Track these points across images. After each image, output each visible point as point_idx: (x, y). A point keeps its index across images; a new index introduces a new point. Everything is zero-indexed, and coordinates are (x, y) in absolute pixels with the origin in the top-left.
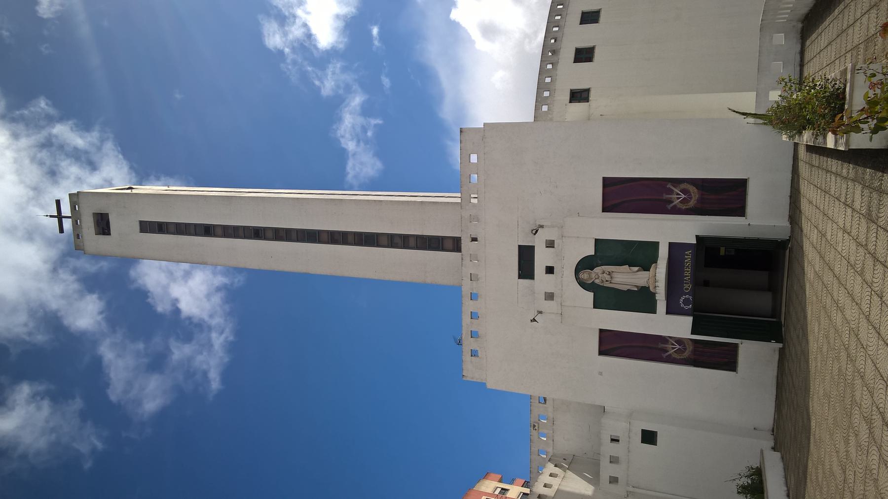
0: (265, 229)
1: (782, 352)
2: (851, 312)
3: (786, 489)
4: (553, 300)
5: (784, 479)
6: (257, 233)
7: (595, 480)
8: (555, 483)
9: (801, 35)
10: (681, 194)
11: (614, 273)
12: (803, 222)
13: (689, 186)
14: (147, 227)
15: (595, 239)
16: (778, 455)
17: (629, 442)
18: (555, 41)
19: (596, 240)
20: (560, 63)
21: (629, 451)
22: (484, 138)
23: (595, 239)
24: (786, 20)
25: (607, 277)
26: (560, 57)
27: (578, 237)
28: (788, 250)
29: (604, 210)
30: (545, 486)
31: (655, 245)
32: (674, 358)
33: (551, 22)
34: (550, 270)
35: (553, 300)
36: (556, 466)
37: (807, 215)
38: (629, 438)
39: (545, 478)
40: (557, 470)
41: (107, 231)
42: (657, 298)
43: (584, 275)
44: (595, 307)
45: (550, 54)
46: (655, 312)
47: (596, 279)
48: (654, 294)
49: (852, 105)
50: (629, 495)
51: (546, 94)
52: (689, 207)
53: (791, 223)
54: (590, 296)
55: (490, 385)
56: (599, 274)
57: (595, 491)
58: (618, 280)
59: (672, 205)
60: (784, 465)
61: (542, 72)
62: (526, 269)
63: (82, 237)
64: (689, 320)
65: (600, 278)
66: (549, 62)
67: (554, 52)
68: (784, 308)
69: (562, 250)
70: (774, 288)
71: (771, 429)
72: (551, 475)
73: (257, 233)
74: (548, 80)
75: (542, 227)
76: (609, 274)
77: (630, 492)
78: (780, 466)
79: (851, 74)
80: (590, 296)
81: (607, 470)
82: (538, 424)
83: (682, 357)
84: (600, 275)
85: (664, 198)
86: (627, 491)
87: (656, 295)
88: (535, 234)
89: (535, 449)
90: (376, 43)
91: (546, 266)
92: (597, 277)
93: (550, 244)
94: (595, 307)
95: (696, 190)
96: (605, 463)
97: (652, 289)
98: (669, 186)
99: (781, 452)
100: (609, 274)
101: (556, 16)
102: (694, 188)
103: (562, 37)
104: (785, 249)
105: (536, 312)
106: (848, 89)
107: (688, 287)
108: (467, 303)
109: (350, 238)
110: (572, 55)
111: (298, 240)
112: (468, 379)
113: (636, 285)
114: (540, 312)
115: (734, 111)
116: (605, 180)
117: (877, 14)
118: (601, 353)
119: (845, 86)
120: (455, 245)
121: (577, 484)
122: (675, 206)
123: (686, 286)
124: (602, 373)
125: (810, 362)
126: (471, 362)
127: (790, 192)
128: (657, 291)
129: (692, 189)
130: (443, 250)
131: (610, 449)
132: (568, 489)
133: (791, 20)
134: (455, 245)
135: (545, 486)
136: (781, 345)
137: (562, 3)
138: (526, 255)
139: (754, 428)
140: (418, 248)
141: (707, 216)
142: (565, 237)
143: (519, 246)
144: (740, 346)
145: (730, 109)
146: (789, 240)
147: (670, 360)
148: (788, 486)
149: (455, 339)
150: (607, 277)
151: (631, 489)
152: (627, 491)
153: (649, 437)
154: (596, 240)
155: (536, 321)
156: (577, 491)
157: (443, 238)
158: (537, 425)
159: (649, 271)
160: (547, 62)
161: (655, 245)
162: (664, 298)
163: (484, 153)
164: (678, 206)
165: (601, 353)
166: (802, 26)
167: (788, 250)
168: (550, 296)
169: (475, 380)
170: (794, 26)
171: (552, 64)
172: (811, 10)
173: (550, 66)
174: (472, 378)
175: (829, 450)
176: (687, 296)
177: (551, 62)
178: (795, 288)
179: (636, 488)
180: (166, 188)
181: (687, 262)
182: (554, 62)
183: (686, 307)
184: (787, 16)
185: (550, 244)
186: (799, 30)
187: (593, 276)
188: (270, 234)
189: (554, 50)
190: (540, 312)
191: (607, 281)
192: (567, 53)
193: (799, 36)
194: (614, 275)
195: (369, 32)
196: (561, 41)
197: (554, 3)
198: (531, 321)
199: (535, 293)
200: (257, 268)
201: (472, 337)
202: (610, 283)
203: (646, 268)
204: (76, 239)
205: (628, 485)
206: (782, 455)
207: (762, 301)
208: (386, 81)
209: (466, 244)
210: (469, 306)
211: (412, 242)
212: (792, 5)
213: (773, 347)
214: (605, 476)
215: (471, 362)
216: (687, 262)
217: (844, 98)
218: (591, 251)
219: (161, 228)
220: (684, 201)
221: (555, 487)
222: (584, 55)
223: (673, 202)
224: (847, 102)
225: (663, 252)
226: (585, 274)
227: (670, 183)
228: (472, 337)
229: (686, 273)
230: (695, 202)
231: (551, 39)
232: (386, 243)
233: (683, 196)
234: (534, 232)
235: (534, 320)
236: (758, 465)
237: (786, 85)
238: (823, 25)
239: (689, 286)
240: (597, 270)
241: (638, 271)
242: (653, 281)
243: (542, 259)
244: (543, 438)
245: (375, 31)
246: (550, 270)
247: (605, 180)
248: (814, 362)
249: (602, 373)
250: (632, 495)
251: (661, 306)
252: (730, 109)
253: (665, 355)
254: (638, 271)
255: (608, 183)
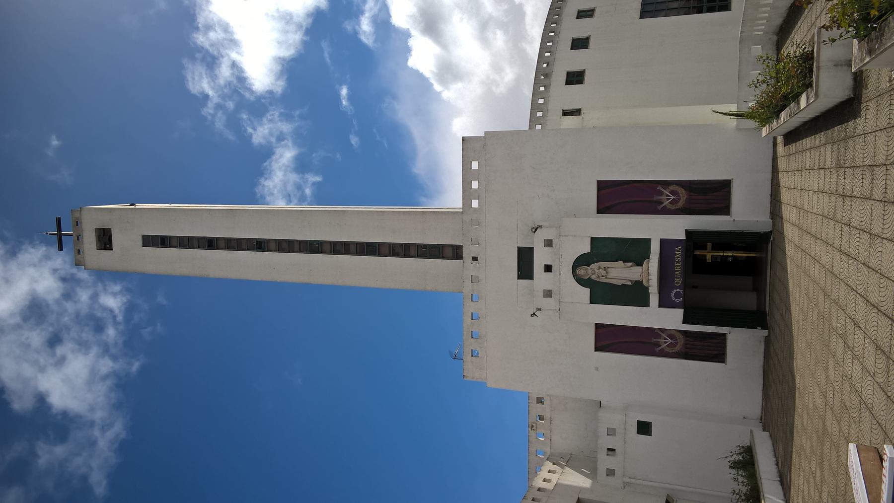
0: (268, 241)
1: (768, 341)
2: (825, 255)
3: (775, 459)
4: (551, 297)
5: (773, 452)
6: (260, 245)
7: (592, 474)
8: (554, 478)
9: (776, 47)
10: (670, 195)
11: (609, 269)
12: (783, 210)
13: (677, 187)
14: (149, 241)
15: (591, 238)
16: (767, 434)
17: (625, 434)
18: (547, 66)
19: (592, 238)
20: (551, 87)
21: (625, 443)
22: (485, 145)
23: (591, 238)
24: (762, 33)
25: (603, 273)
26: (552, 79)
27: (575, 236)
28: (770, 243)
29: (599, 211)
30: (544, 480)
31: (647, 242)
32: (667, 352)
33: (543, 48)
34: (548, 268)
35: (551, 297)
36: (554, 464)
37: (790, 238)
38: (625, 429)
39: (544, 474)
40: (555, 467)
41: (108, 246)
42: (650, 291)
43: (581, 271)
44: (591, 303)
45: (542, 77)
46: (648, 306)
47: (593, 274)
48: (647, 288)
49: (819, 61)
50: (626, 487)
51: (540, 114)
52: (678, 207)
53: (772, 219)
54: (586, 292)
55: (491, 384)
56: (595, 271)
57: (593, 484)
58: (612, 275)
59: (662, 206)
60: (772, 441)
61: (536, 94)
62: (525, 267)
63: (83, 252)
64: (681, 311)
65: (596, 274)
66: (541, 85)
67: (547, 76)
68: (768, 298)
69: (559, 248)
70: (758, 289)
71: (760, 417)
72: (549, 471)
73: (260, 245)
74: (541, 101)
75: (540, 227)
76: (605, 269)
77: (627, 482)
78: (769, 443)
79: (818, 36)
80: (586, 292)
81: (605, 462)
82: (536, 424)
83: (674, 351)
84: (597, 271)
85: (655, 199)
86: (624, 482)
87: (649, 288)
88: (535, 232)
89: (533, 450)
90: (344, 102)
91: (545, 265)
92: (593, 272)
93: (549, 243)
94: (591, 303)
95: (684, 191)
96: (602, 455)
97: (645, 283)
98: (659, 188)
99: (769, 432)
100: (605, 269)
101: (547, 42)
102: (683, 190)
103: (554, 61)
104: (767, 242)
105: (535, 309)
106: (815, 50)
107: (678, 281)
108: (468, 305)
109: (353, 248)
110: (563, 78)
111: (300, 251)
112: (468, 379)
113: (630, 279)
114: (539, 309)
115: (718, 112)
116: (599, 183)
117: (866, 118)
118: (597, 349)
119: (813, 47)
120: (456, 252)
121: (576, 479)
122: (665, 206)
123: (677, 280)
124: (597, 368)
125: (793, 328)
126: (472, 362)
127: (770, 191)
128: (650, 284)
129: (681, 191)
130: (443, 257)
131: (607, 442)
132: (566, 483)
133: (767, 33)
134: (456, 252)
135: (544, 480)
136: (765, 333)
137: (553, 30)
138: (525, 258)
139: (744, 417)
140: (418, 256)
141: (695, 216)
142: (563, 236)
143: (519, 248)
144: (729, 337)
145: (713, 111)
146: (771, 232)
147: (663, 354)
148: (777, 457)
149: (450, 353)
150: (603, 273)
151: (627, 480)
152: (624, 482)
153: (644, 428)
154: (592, 238)
155: (536, 315)
156: (575, 484)
157: (443, 246)
158: (534, 425)
159: (642, 266)
160: (540, 85)
161: (647, 242)
162: (657, 292)
163: (485, 160)
164: (668, 207)
165: (597, 349)
166: (777, 38)
167: (770, 243)
168: (548, 294)
169: (475, 380)
170: (770, 39)
171: (544, 86)
172: (784, 21)
173: (542, 89)
174: (473, 378)
175: (811, 391)
176: (678, 290)
177: (544, 84)
178: (778, 274)
179: (632, 478)
180: (169, 205)
181: (677, 258)
182: (546, 84)
183: (677, 301)
184: (764, 27)
185: (549, 243)
186: (775, 43)
187: (590, 271)
188: (273, 246)
189: (547, 74)
190: (539, 309)
191: (602, 276)
192: (559, 77)
193: (775, 48)
194: (610, 270)
195: (338, 97)
196: (553, 65)
197: (546, 30)
198: (531, 315)
199: (534, 291)
200: (259, 280)
201: (472, 338)
202: (606, 278)
203: (640, 264)
204: (77, 255)
205: (624, 476)
206: (770, 434)
207: (747, 301)
208: (354, 140)
209: (467, 253)
210: (470, 307)
211: (413, 251)
212: (767, 15)
213: (761, 333)
214: (602, 469)
215: (472, 362)
216: (677, 258)
217: (812, 58)
218: (587, 249)
219: (163, 242)
220: (673, 202)
221: (554, 482)
222: (575, 78)
223: (662, 203)
224: (815, 60)
225: (655, 248)
226: (582, 270)
227: (660, 186)
228: (472, 338)
229: (677, 268)
230: (684, 202)
231: (544, 64)
232: (387, 252)
233: (673, 197)
234: (533, 230)
235: (534, 315)
236: (749, 444)
237: (764, 61)
238: (795, 28)
239: (680, 280)
240: (593, 266)
241: (632, 266)
242: (646, 275)
243: (540, 259)
244: (540, 439)
245: (344, 92)
246: (548, 268)
247: (599, 183)
248: (796, 325)
249: (597, 368)
250: (629, 486)
251: (654, 299)
252: (713, 111)
253: (658, 349)
254: (632, 266)
255: (602, 186)
